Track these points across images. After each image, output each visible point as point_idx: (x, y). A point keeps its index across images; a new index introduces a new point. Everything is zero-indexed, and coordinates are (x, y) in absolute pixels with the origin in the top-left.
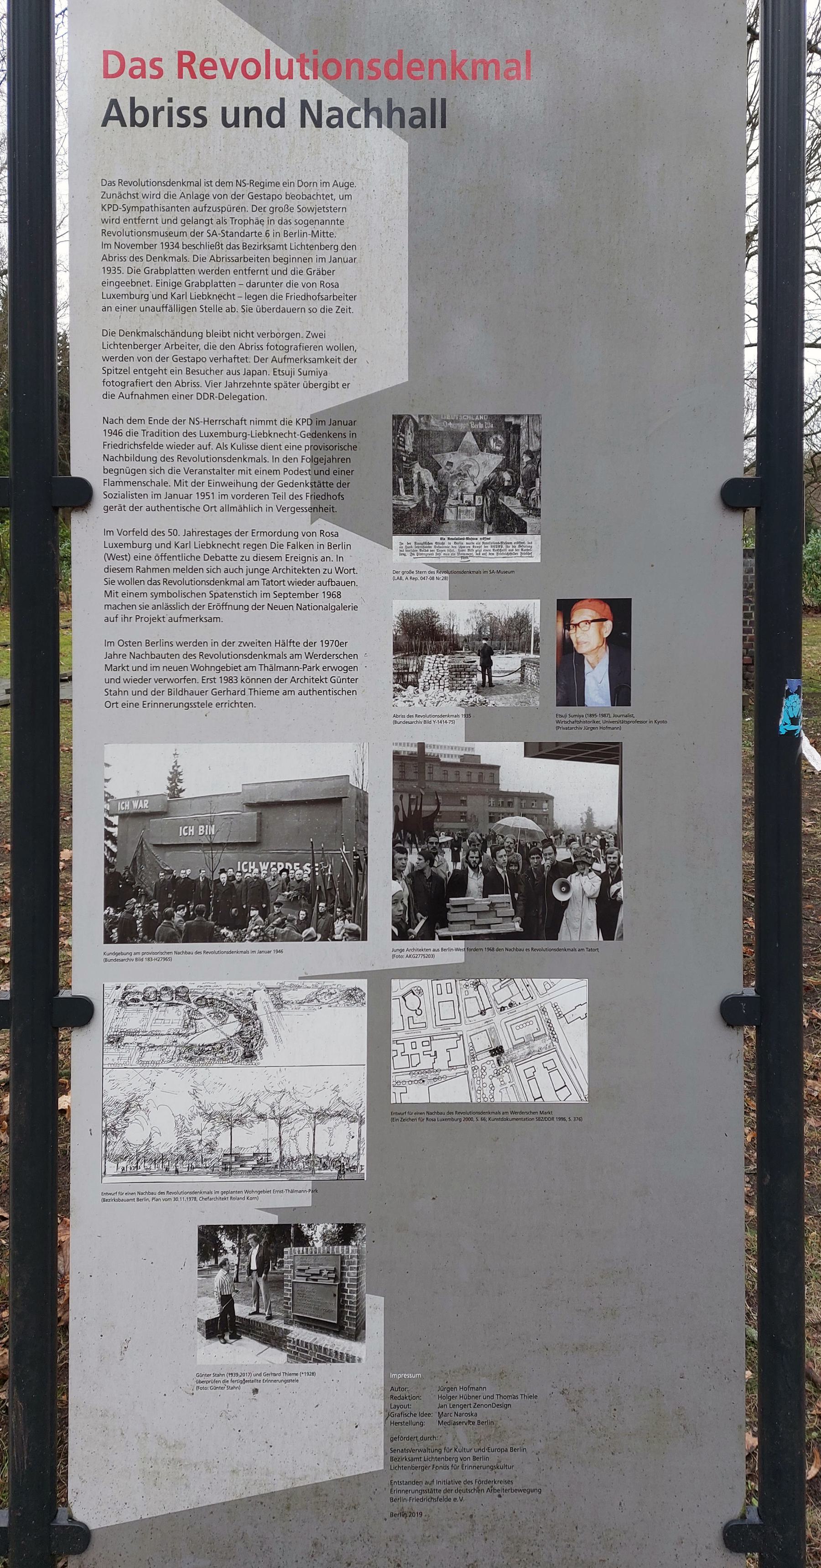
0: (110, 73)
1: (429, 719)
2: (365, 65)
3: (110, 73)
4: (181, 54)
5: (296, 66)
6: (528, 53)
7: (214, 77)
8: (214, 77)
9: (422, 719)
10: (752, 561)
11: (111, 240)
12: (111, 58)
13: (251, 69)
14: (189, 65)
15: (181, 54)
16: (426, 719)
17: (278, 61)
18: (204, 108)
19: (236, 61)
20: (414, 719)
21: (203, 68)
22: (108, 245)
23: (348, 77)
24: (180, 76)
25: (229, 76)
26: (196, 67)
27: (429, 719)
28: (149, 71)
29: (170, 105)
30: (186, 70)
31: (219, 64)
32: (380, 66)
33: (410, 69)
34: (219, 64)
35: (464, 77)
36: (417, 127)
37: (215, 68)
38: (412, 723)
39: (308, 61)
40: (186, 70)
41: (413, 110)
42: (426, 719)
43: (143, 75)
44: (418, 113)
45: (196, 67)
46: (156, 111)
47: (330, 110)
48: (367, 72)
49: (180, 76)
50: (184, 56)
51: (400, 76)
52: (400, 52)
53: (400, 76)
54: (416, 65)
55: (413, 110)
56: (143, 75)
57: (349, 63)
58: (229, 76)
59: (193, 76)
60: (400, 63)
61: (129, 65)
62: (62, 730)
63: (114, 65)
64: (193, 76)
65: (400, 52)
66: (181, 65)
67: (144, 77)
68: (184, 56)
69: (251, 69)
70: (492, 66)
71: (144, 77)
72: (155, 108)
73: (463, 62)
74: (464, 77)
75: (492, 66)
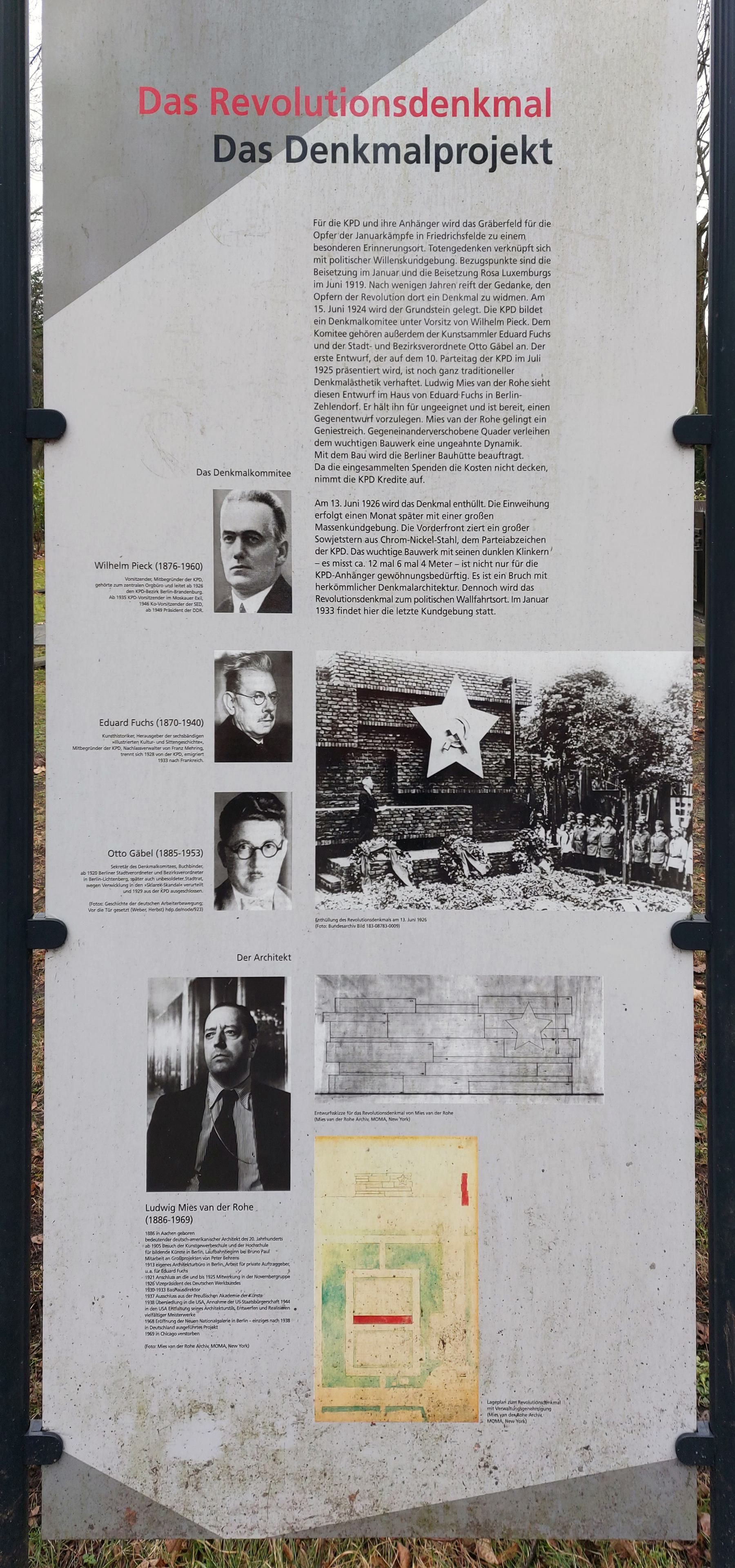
0: (146, 109)
1: (362, 923)
2: (182, 99)
3: (146, 109)
4: (214, 91)
5: (325, 104)
6: (548, 91)
7: (246, 113)
8: (246, 113)
9: (355, 923)
10: (37, 660)
11: (323, 279)
12: (147, 94)
13: (282, 106)
14: (222, 102)
15: (214, 91)
16: (360, 923)
17: (307, 98)
18: (269, 144)
19: (267, 98)
20: (347, 923)
21: (235, 105)
22: (320, 284)
23: (375, 114)
24: (214, 112)
25: (261, 112)
26: (229, 103)
27: (362, 923)
28: (184, 107)
29: (494, 142)
30: (219, 107)
31: (251, 102)
32: (407, 104)
33: (434, 107)
34: (251, 102)
35: (486, 114)
36: (411, 162)
37: (246, 104)
38: (345, 927)
39: (336, 98)
40: (219, 107)
41: (408, 146)
42: (360, 923)
43: (178, 111)
44: (413, 149)
45: (229, 103)
46: (460, 148)
47: (243, 144)
48: (393, 109)
49: (214, 112)
50: (217, 93)
51: (424, 113)
52: (425, 90)
53: (424, 113)
54: (241, 101)
55: (408, 146)
56: (178, 111)
57: (376, 100)
58: (261, 112)
59: (226, 112)
60: (424, 100)
61: (164, 101)
62: (36, 876)
63: (150, 101)
64: (226, 112)
65: (425, 90)
66: (214, 102)
67: (179, 113)
68: (217, 93)
69: (282, 106)
70: (513, 104)
71: (179, 113)
72: (459, 146)
73: (486, 99)
74: (486, 114)
75: (513, 104)
